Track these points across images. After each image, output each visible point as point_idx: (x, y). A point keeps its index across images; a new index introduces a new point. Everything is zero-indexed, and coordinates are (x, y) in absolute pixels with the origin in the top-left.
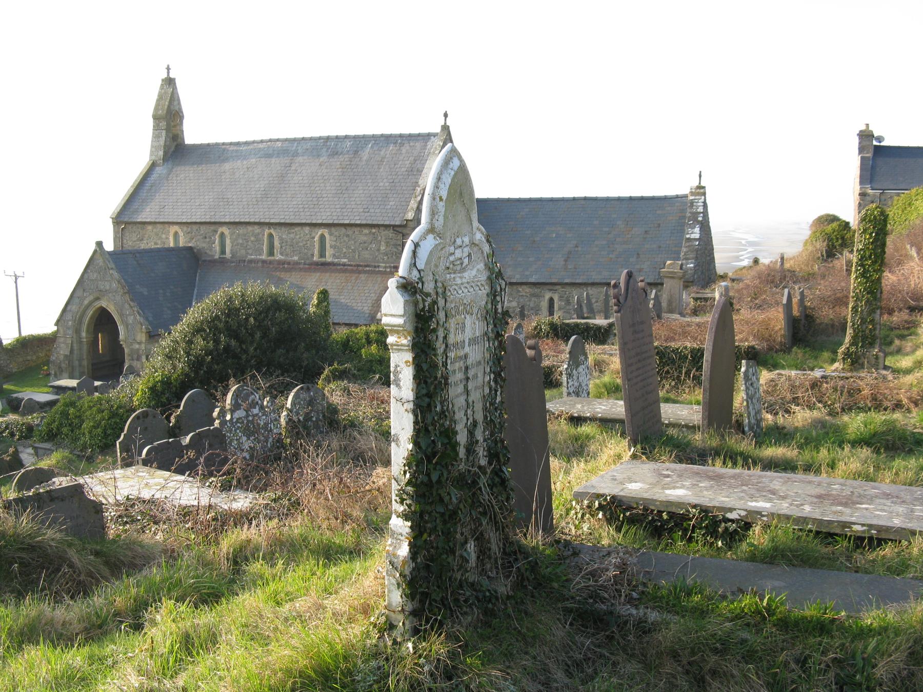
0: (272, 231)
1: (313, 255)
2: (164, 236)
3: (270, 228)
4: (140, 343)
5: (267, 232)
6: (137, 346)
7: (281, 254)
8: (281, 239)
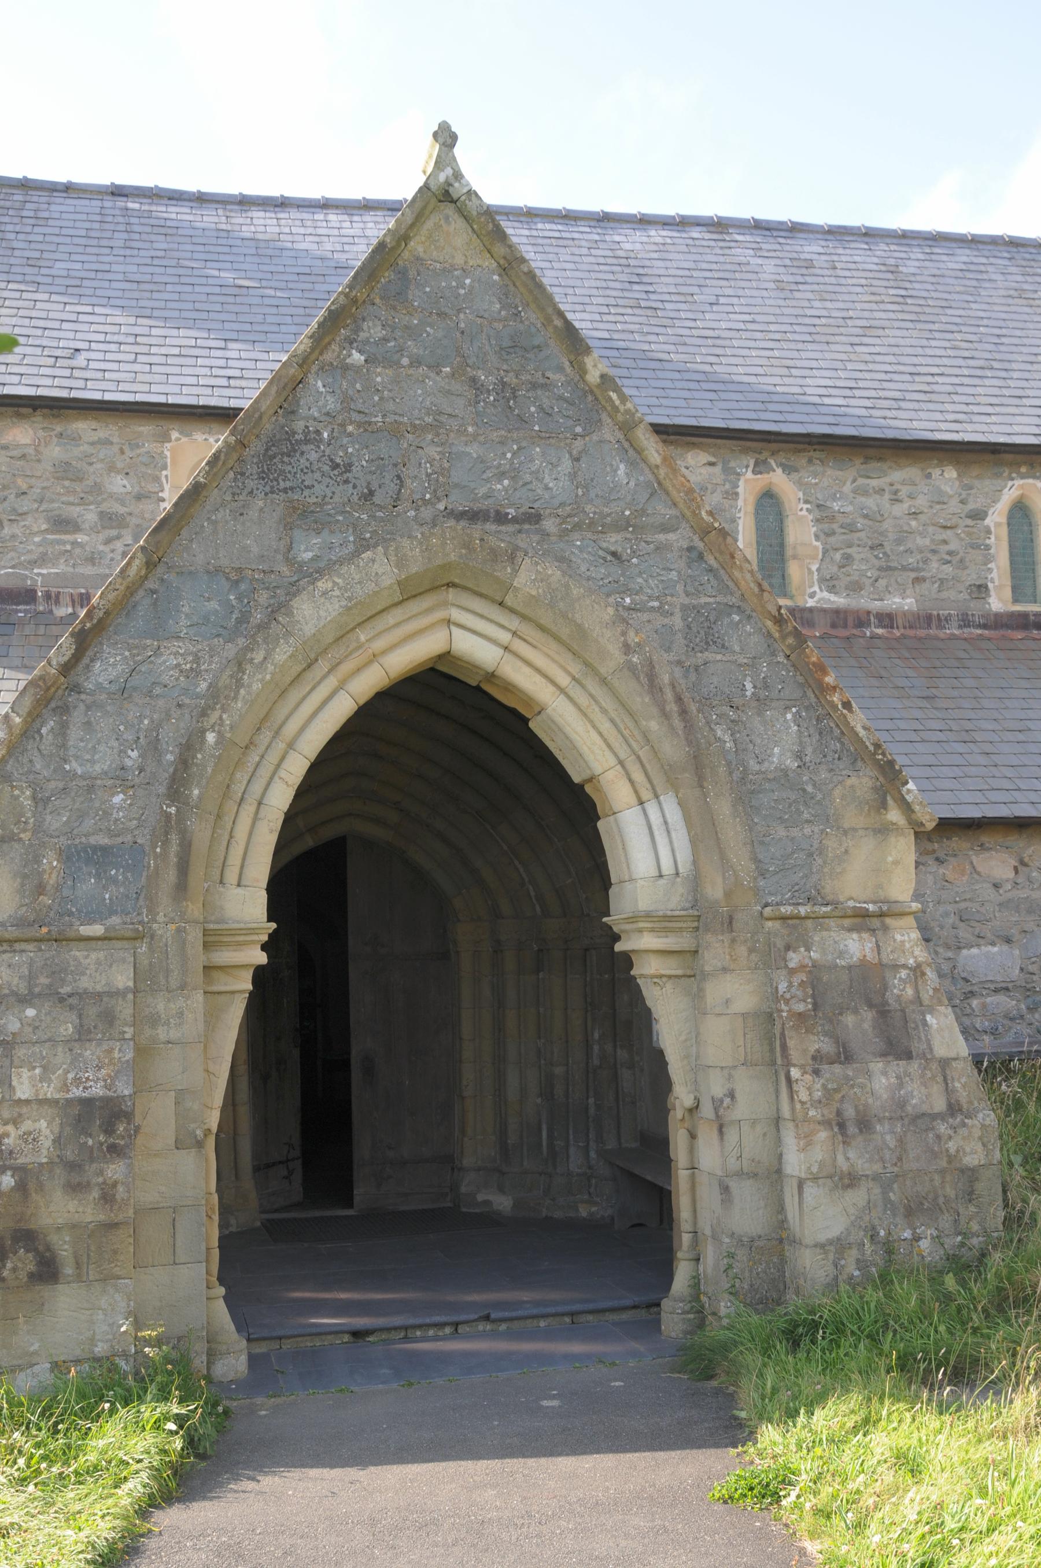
0: (778, 478)
1: (981, 590)
2: (119, 484)
3: (760, 467)
4: (869, 919)
5: (749, 484)
6: (857, 947)
7: (830, 584)
8: (824, 515)
